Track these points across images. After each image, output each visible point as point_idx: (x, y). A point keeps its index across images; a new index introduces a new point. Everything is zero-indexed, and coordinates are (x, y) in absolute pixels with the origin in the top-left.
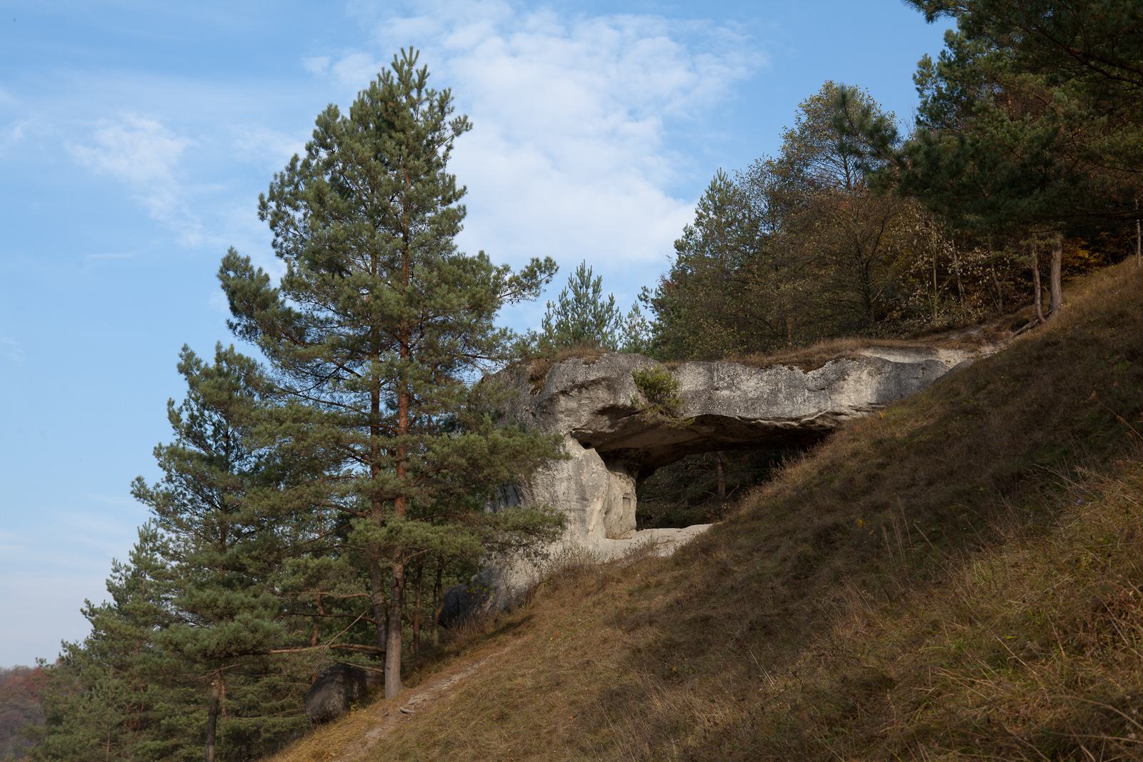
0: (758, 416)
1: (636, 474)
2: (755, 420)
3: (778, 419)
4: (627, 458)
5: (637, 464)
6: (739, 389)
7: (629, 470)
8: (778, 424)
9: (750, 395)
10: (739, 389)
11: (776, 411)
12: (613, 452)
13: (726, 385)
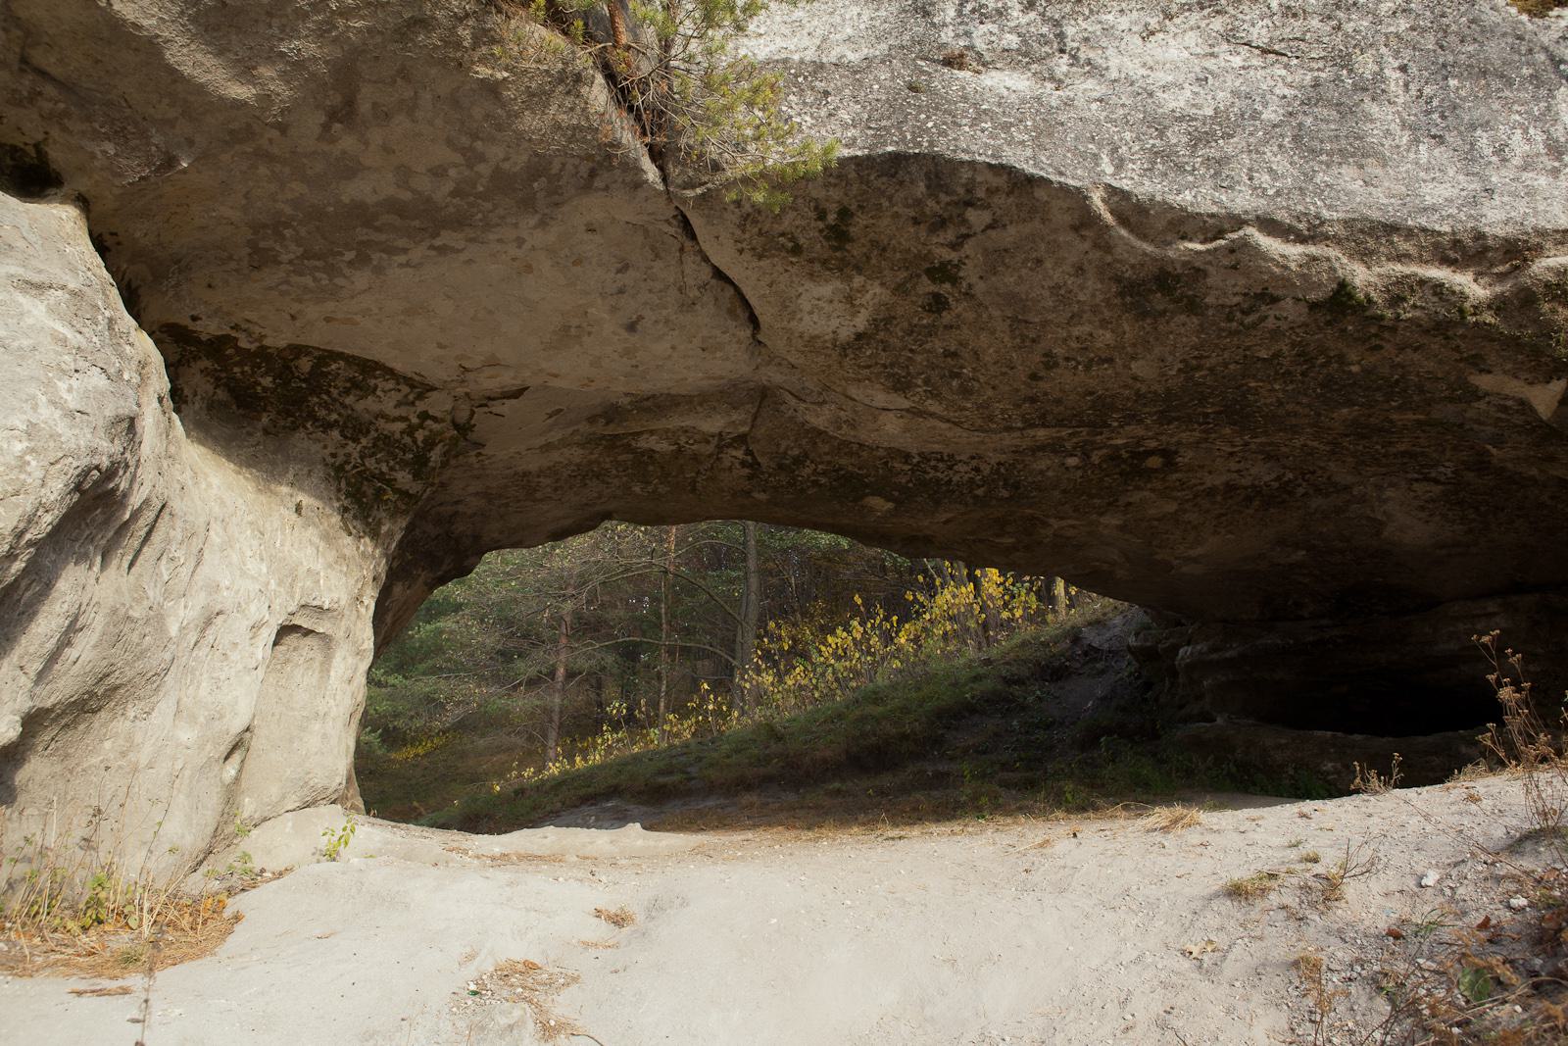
0: (1242, 201)
1: (395, 528)
2: (1214, 227)
3: (1371, 235)
4: (354, 429)
5: (403, 478)
6: (1094, 70)
7: (359, 498)
8: (1362, 276)
9: (1175, 102)
10: (1094, 70)
11: (1353, 192)
12: (282, 362)
13: (1012, 40)
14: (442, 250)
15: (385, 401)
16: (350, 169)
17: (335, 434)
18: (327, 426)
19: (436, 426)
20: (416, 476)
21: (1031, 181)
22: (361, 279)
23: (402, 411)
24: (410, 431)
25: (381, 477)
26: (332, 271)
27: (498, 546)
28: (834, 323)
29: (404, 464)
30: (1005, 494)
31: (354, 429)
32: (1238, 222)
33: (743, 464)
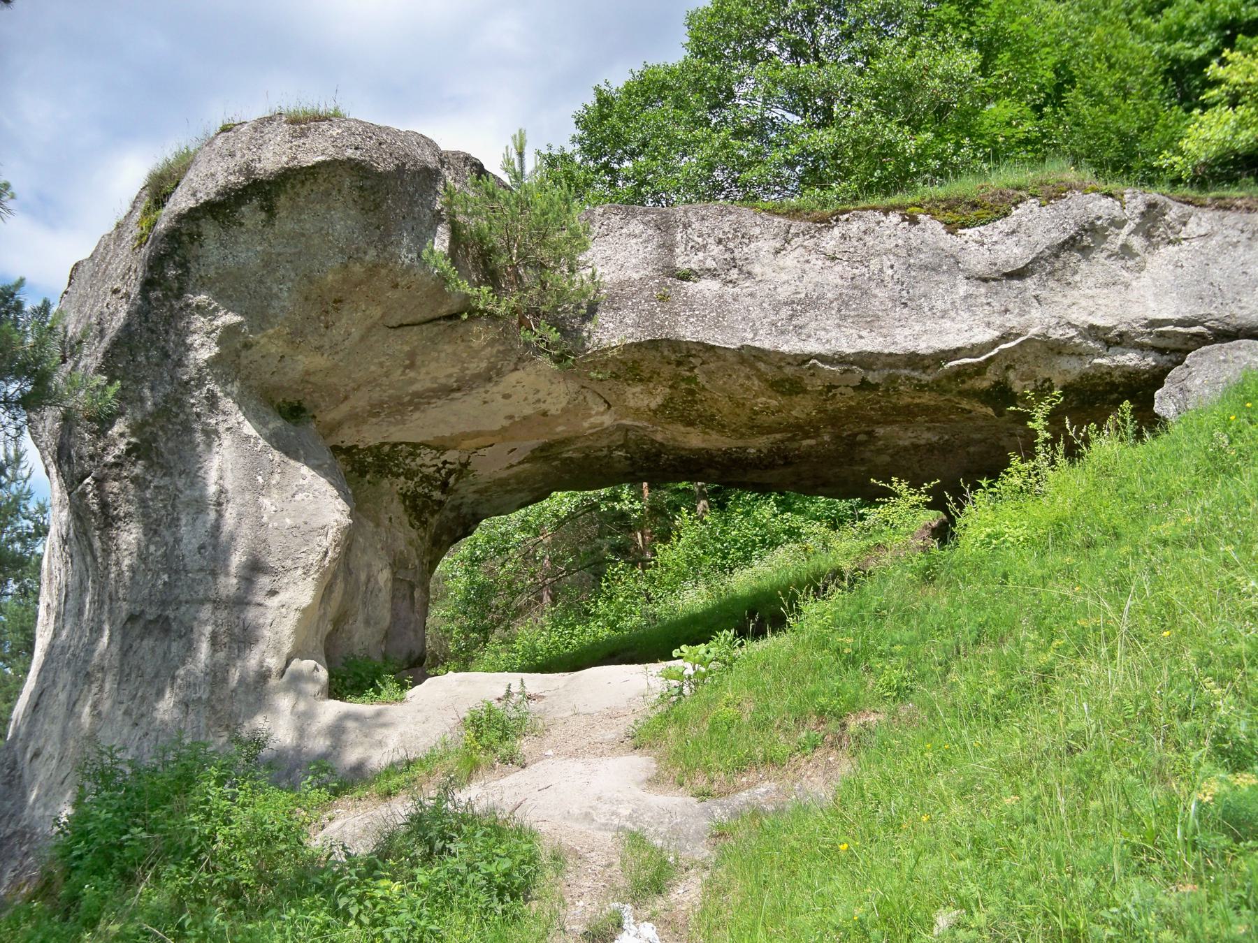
4: (409, 475)
12: (376, 451)
14: (452, 399)
15: (426, 458)
16: (412, 382)
17: (402, 478)
18: (398, 476)
19: (451, 467)
20: (443, 493)
21: (713, 347)
22: (417, 415)
23: (434, 462)
24: (439, 470)
25: (425, 495)
26: (402, 414)
27: (487, 516)
28: (646, 402)
29: (436, 488)
30: (781, 462)
31: (409, 475)
32: (811, 356)
33: (626, 458)
